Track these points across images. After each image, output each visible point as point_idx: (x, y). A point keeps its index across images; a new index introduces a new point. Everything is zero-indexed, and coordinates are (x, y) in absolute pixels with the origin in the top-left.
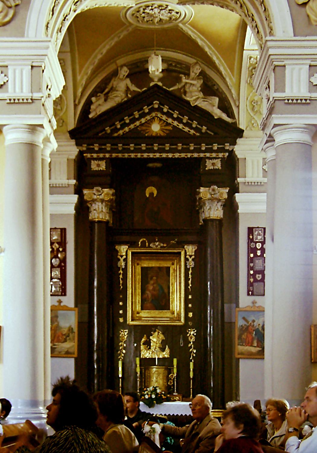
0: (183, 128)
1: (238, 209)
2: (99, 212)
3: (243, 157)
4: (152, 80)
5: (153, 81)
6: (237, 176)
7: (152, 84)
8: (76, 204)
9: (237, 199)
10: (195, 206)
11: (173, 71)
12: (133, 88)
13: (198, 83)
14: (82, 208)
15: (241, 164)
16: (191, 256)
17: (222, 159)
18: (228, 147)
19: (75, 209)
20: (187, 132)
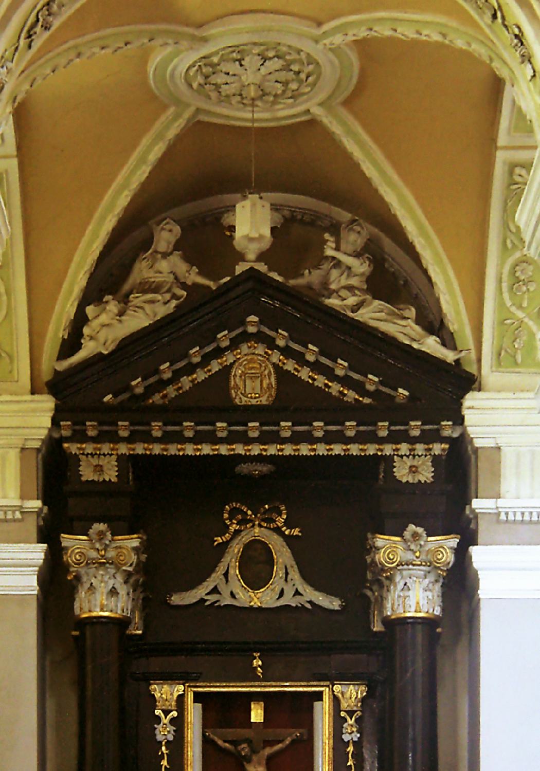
0: (326, 385)
1: (478, 589)
2: (104, 598)
3: (489, 443)
4: (241, 257)
5: (244, 260)
6: (473, 493)
7: (240, 269)
8: (45, 553)
9: (475, 559)
10: (360, 581)
11: (296, 240)
12: (194, 277)
13: (361, 267)
14: (57, 582)
15: (483, 465)
16: (351, 713)
17: (436, 460)
18: (448, 429)
19: (41, 582)
20: (337, 394)
